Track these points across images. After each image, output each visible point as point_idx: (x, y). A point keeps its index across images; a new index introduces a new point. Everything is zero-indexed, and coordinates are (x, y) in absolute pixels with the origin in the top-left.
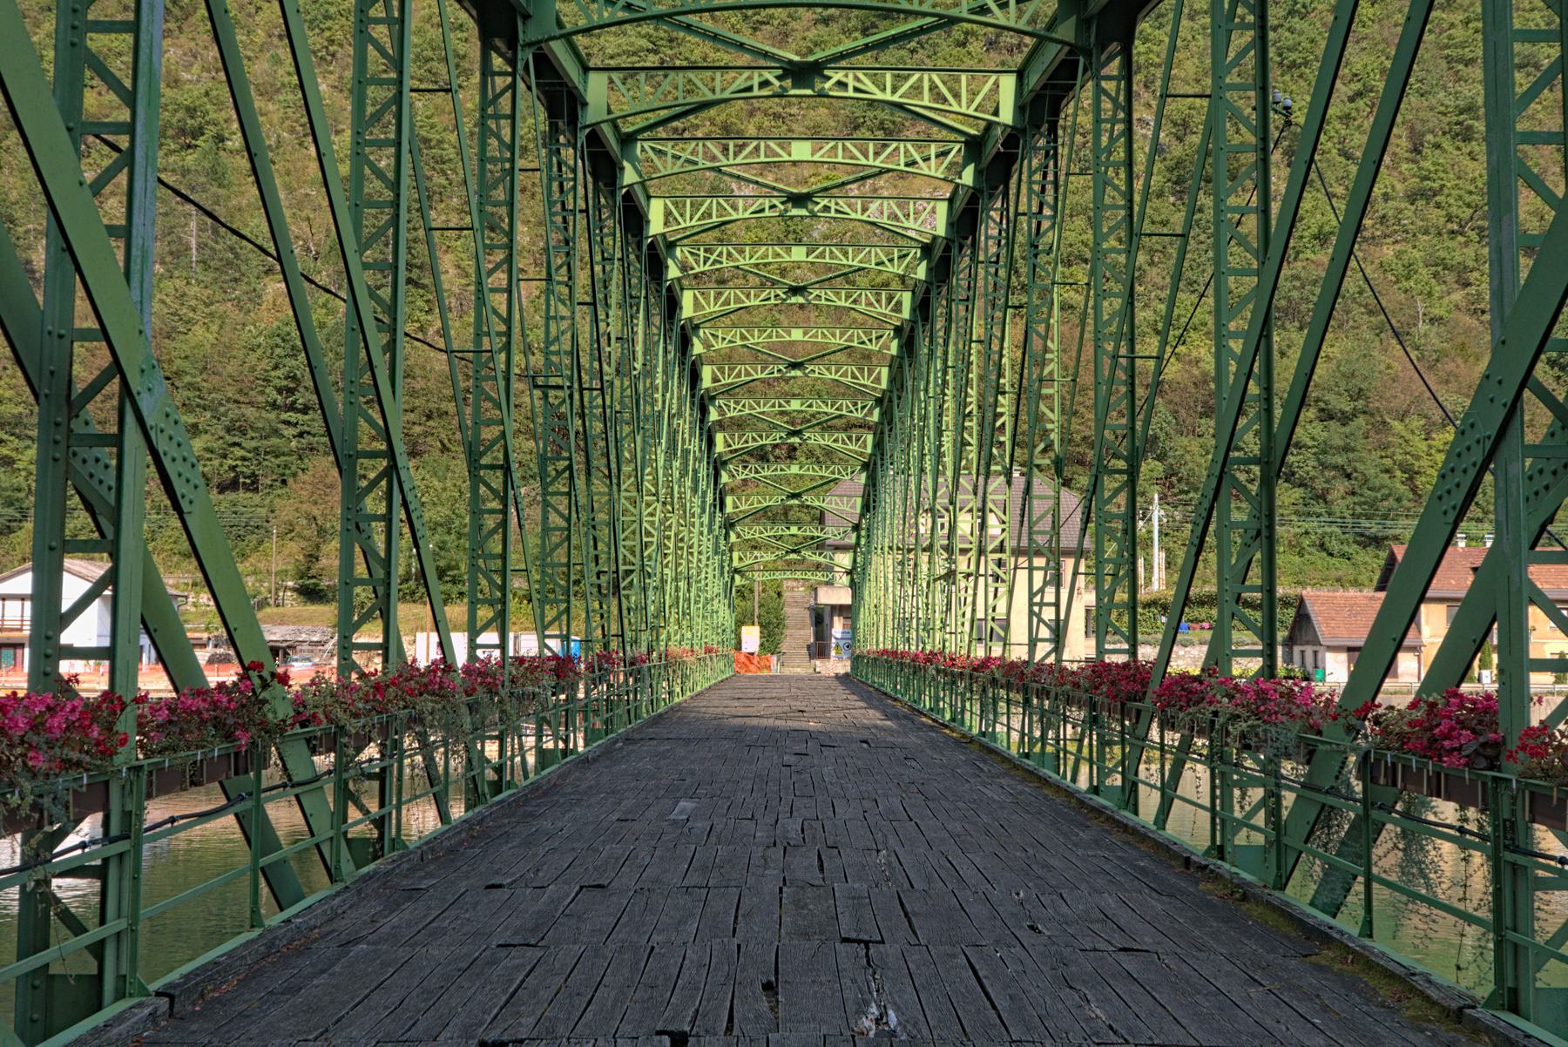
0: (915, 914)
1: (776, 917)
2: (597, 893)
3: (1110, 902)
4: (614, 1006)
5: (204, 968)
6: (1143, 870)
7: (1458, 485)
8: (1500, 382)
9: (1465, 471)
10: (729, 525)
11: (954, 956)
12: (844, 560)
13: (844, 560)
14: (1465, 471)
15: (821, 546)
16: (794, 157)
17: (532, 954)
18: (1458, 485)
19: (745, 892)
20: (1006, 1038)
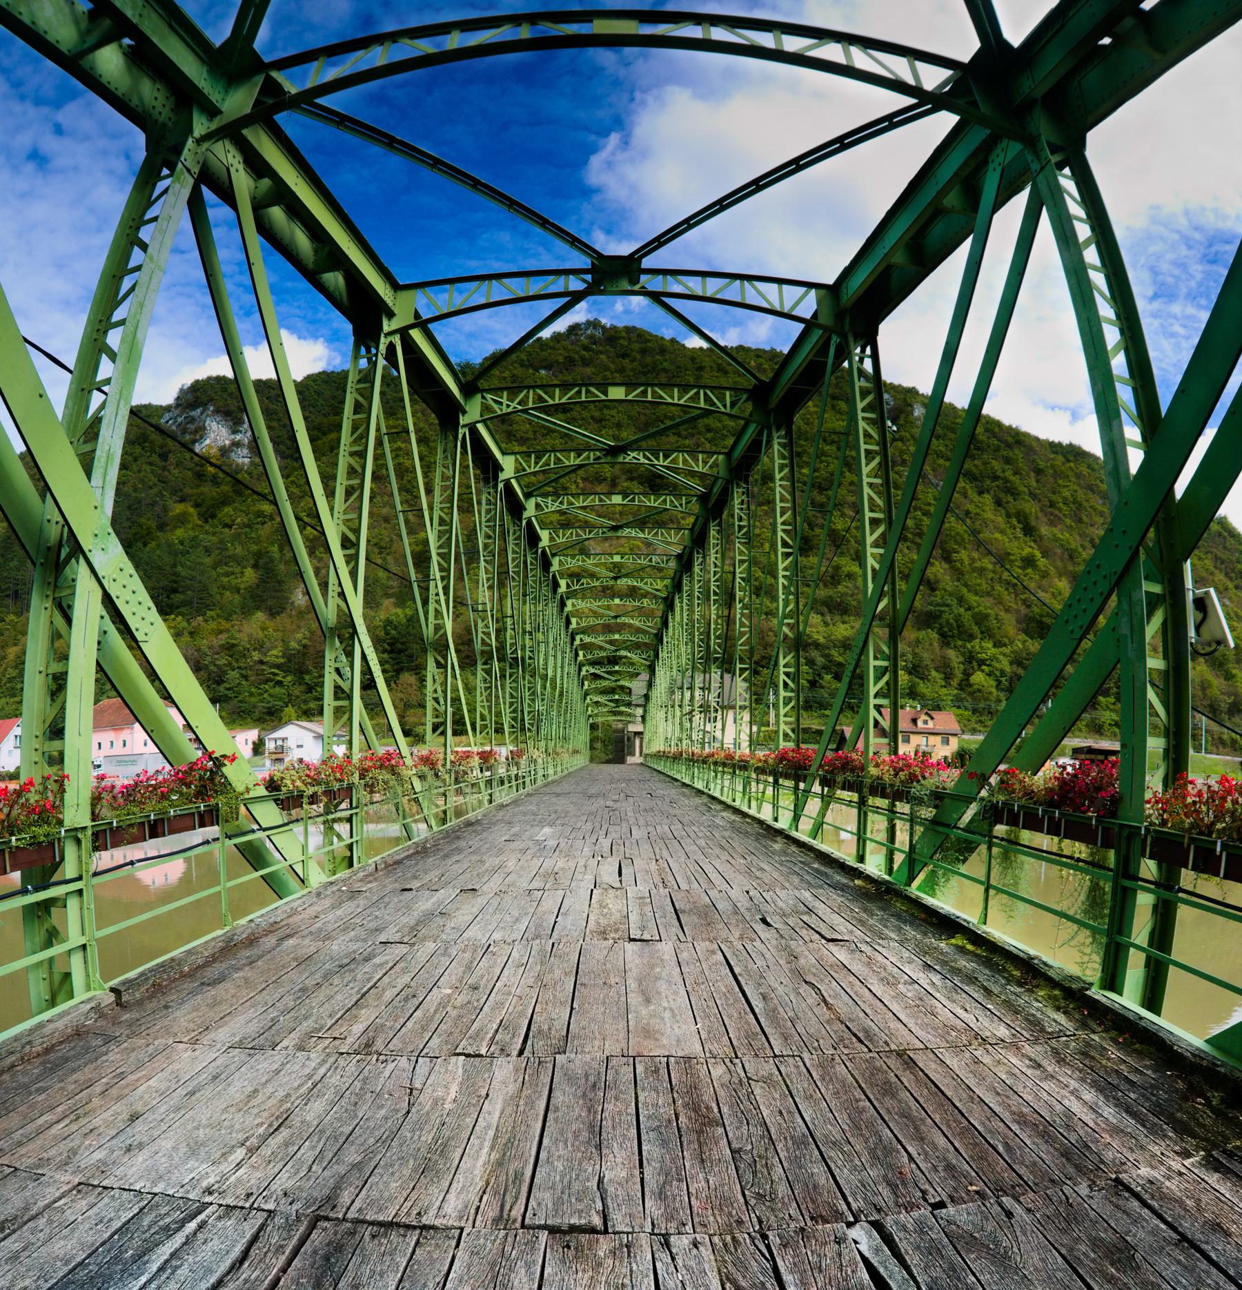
0: (683, 912)
1: (585, 915)
2: (470, 894)
3: (806, 895)
4: (436, 1012)
5: (162, 965)
6: (817, 870)
7: (1085, 611)
8: (1124, 532)
9: (1092, 600)
10: (586, 694)
11: (713, 952)
12: (640, 711)
13: (640, 711)
14: (1092, 600)
15: (629, 704)
16: (610, 397)
17: (403, 949)
18: (1085, 611)
19: (568, 893)
20: (768, 1051)
